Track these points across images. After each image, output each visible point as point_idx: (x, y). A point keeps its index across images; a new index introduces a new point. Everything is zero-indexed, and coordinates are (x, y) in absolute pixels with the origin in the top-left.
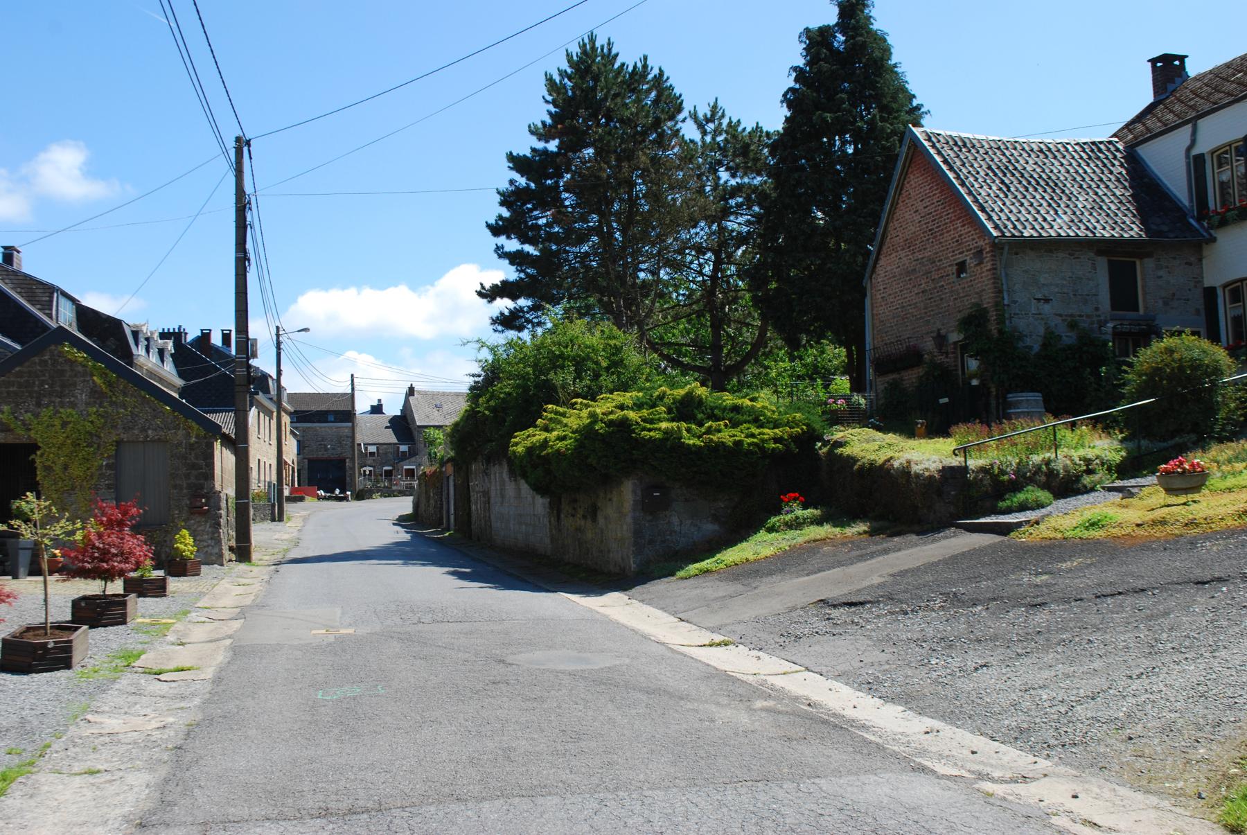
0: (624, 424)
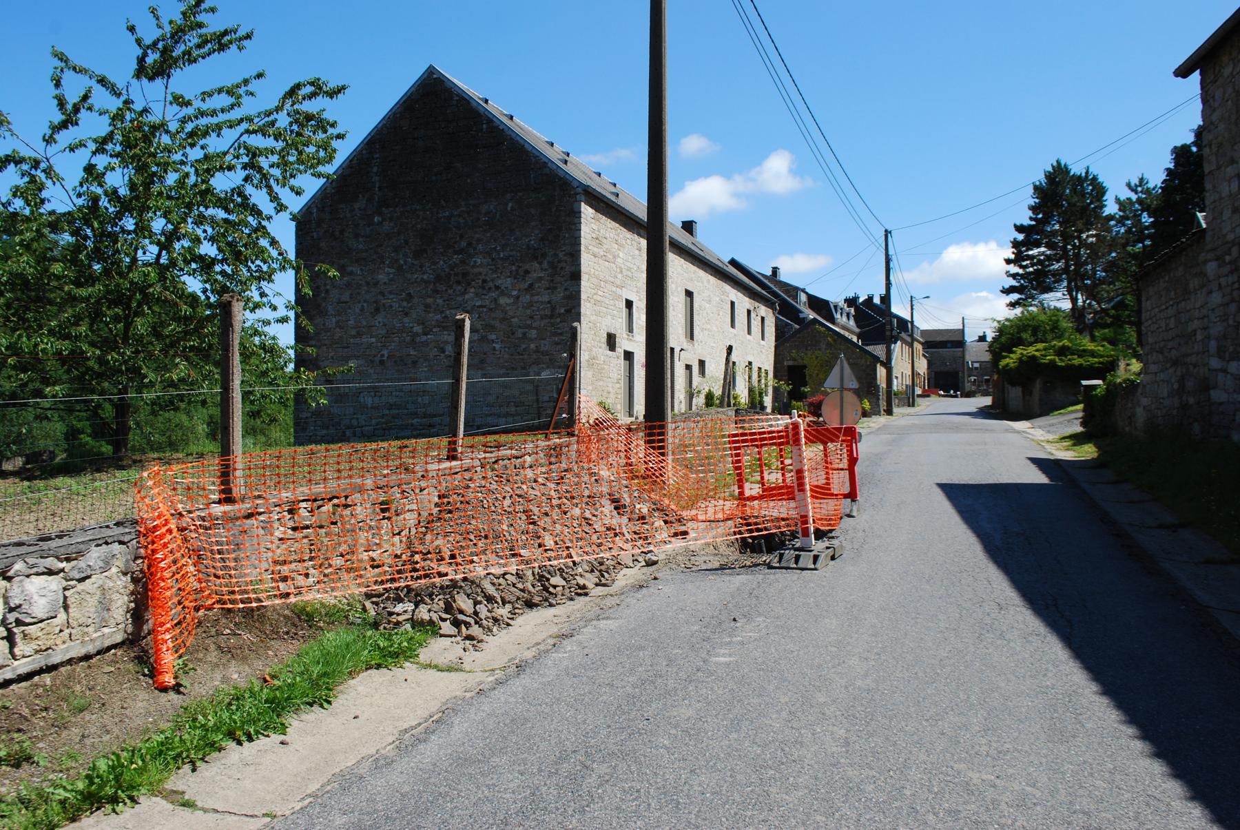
0: (1034, 357)
